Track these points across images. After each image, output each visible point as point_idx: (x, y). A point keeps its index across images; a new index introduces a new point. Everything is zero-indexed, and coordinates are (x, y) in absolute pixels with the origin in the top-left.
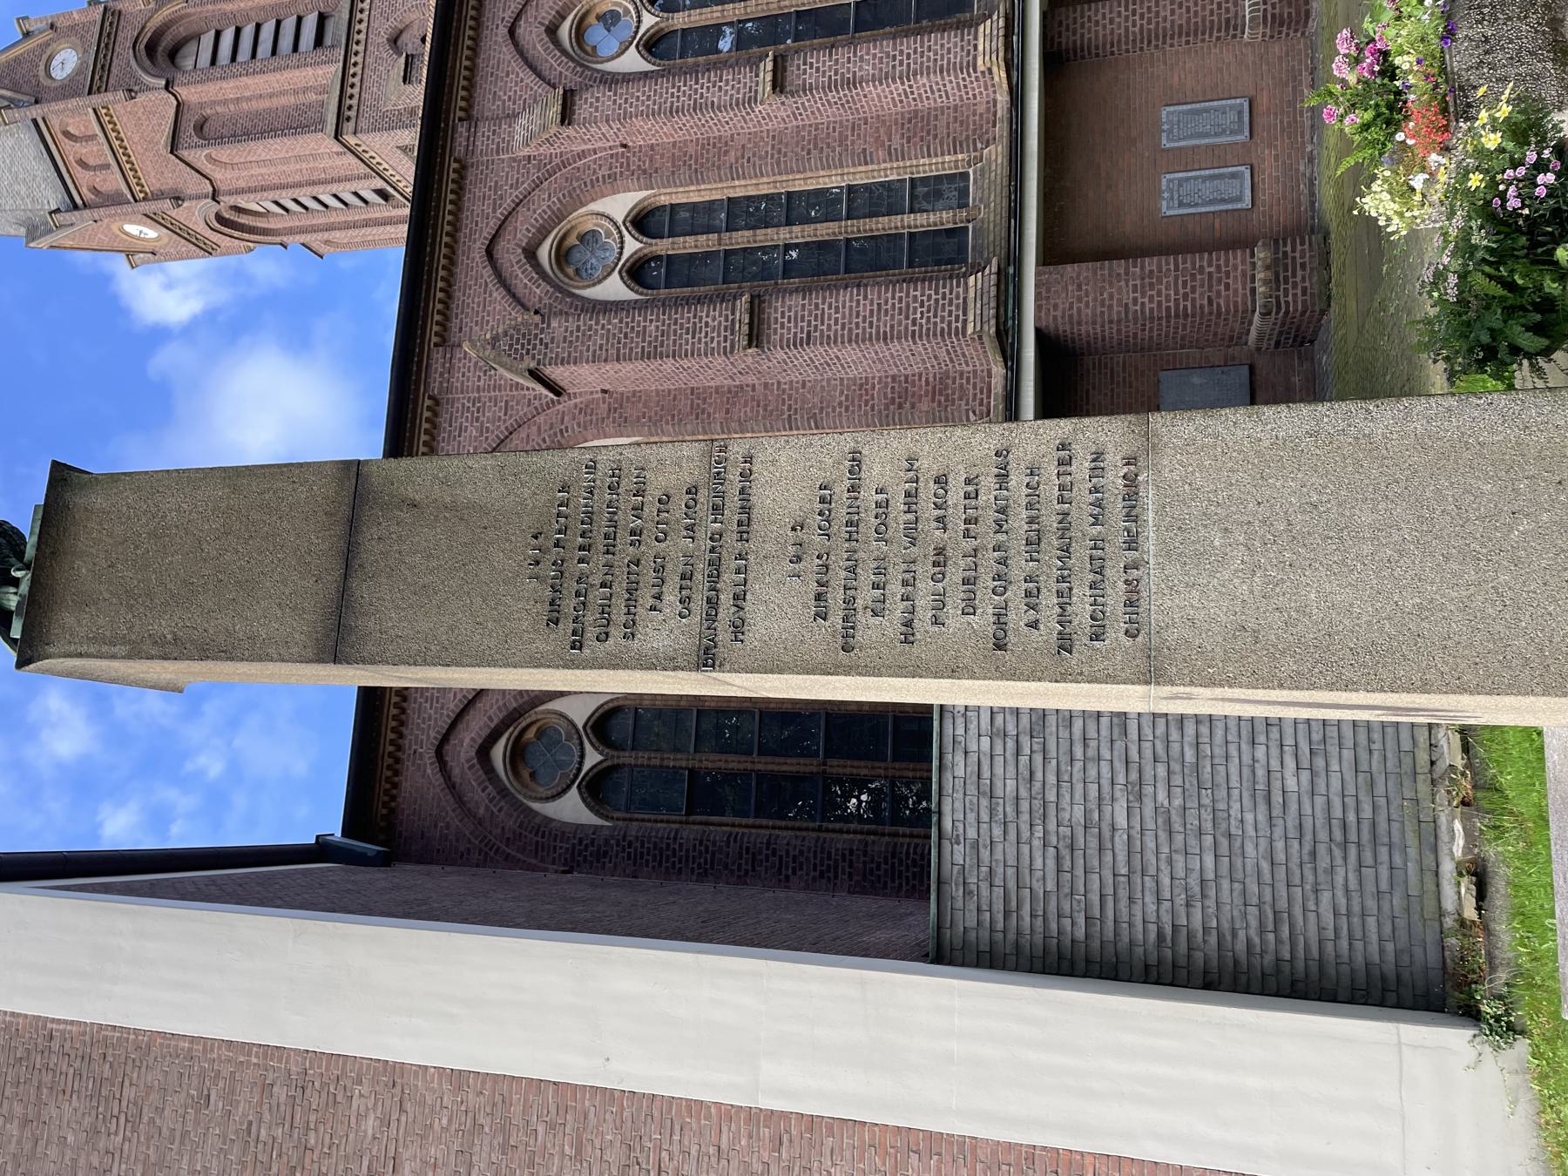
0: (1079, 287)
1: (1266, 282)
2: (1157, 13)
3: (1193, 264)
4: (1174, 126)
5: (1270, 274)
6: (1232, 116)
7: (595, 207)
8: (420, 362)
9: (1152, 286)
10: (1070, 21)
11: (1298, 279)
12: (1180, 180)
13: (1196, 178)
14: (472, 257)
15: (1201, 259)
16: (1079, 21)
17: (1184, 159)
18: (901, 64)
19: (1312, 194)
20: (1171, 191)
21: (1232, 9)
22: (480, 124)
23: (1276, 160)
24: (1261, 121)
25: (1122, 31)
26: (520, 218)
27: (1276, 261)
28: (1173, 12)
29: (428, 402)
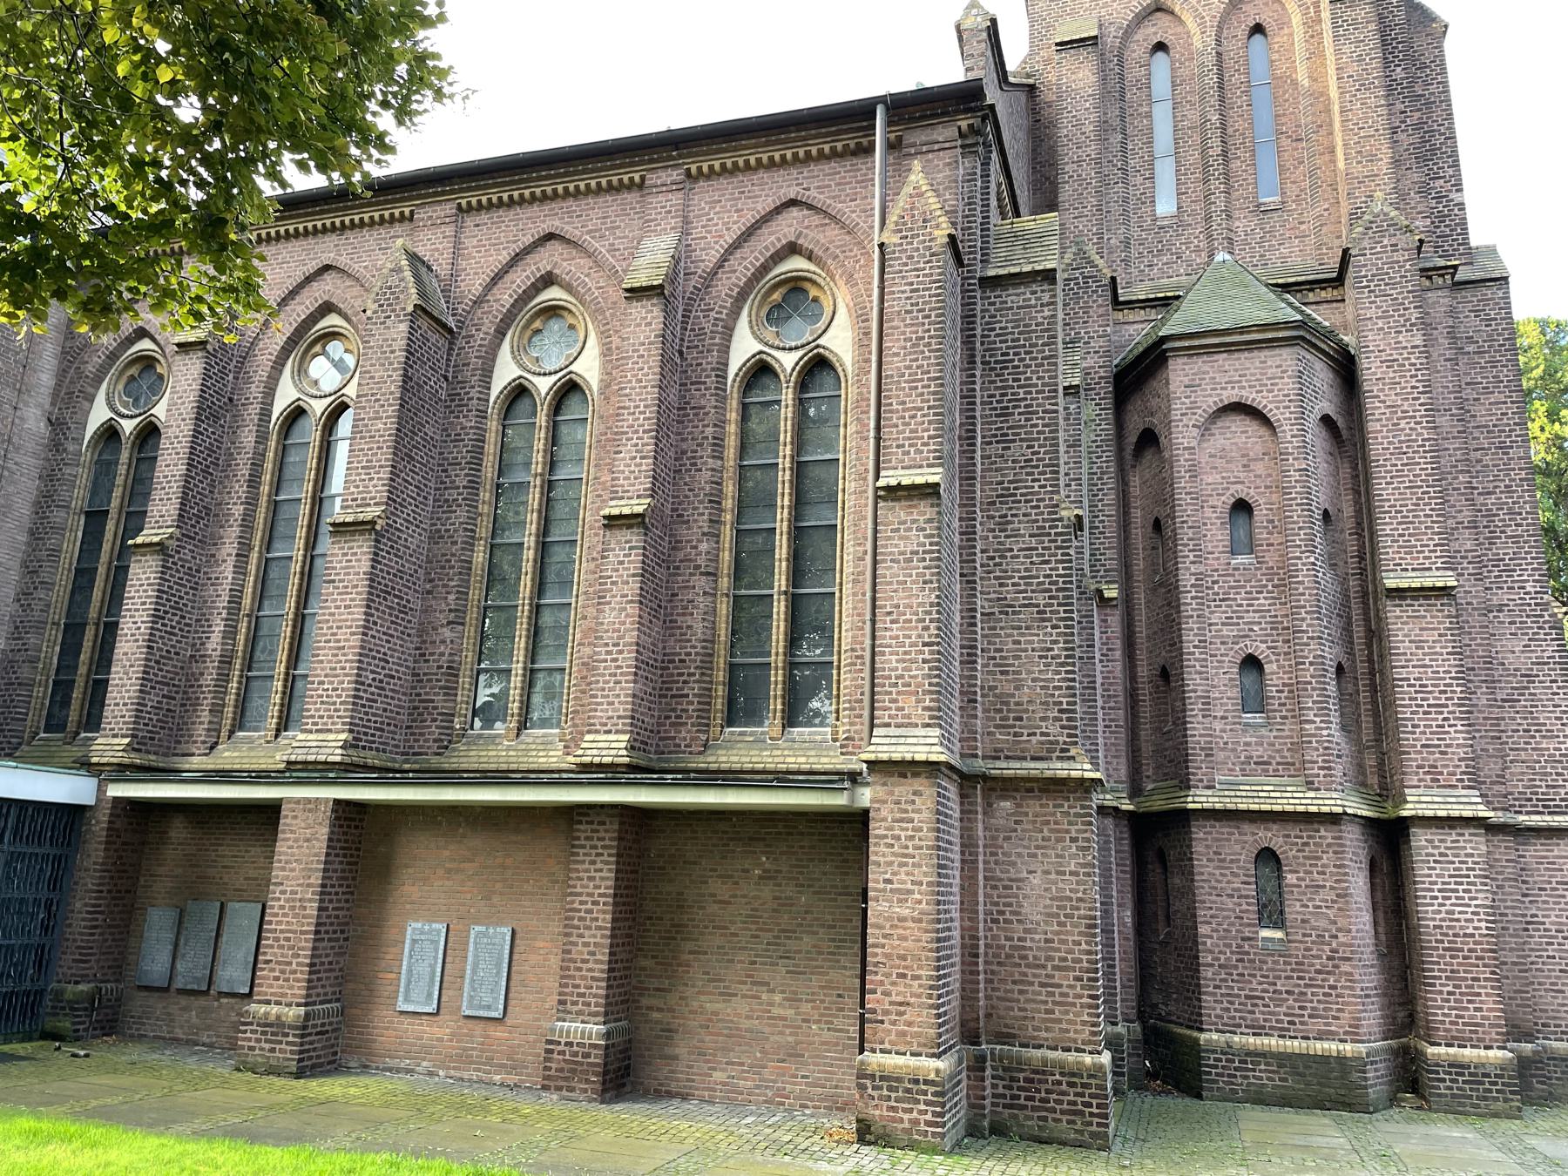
0: (308, 840)
1: (267, 1014)
2: (589, 928)
3: (302, 949)
4: (488, 941)
5: (272, 1018)
6: (487, 1000)
7: (592, 340)
8: (443, 193)
9: (293, 908)
10: (602, 834)
11: (263, 1045)
12: (437, 942)
13: (436, 958)
14: (785, 185)
15: (305, 956)
16: (600, 844)
17: (452, 949)
18: (608, 653)
19: (398, 1071)
20: (430, 932)
21: (575, 1008)
22: (680, 195)
23: (438, 1039)
24: (479, 1028)
25: (579, 890)
26: (582, 262)
27: (283, 1025)
28: (586, 944)
29: (407, 211)
